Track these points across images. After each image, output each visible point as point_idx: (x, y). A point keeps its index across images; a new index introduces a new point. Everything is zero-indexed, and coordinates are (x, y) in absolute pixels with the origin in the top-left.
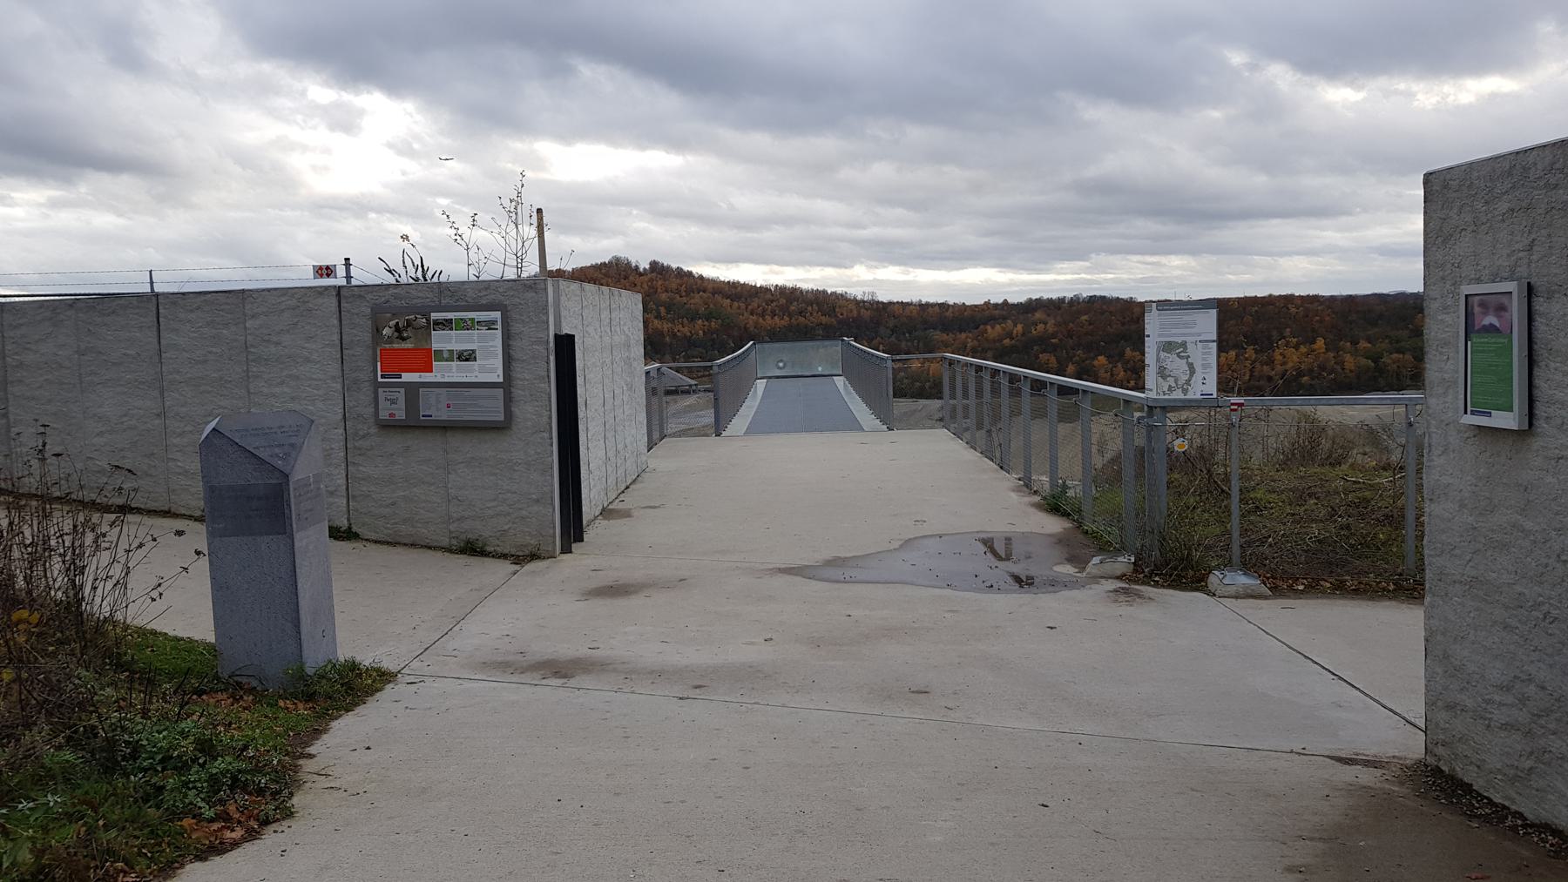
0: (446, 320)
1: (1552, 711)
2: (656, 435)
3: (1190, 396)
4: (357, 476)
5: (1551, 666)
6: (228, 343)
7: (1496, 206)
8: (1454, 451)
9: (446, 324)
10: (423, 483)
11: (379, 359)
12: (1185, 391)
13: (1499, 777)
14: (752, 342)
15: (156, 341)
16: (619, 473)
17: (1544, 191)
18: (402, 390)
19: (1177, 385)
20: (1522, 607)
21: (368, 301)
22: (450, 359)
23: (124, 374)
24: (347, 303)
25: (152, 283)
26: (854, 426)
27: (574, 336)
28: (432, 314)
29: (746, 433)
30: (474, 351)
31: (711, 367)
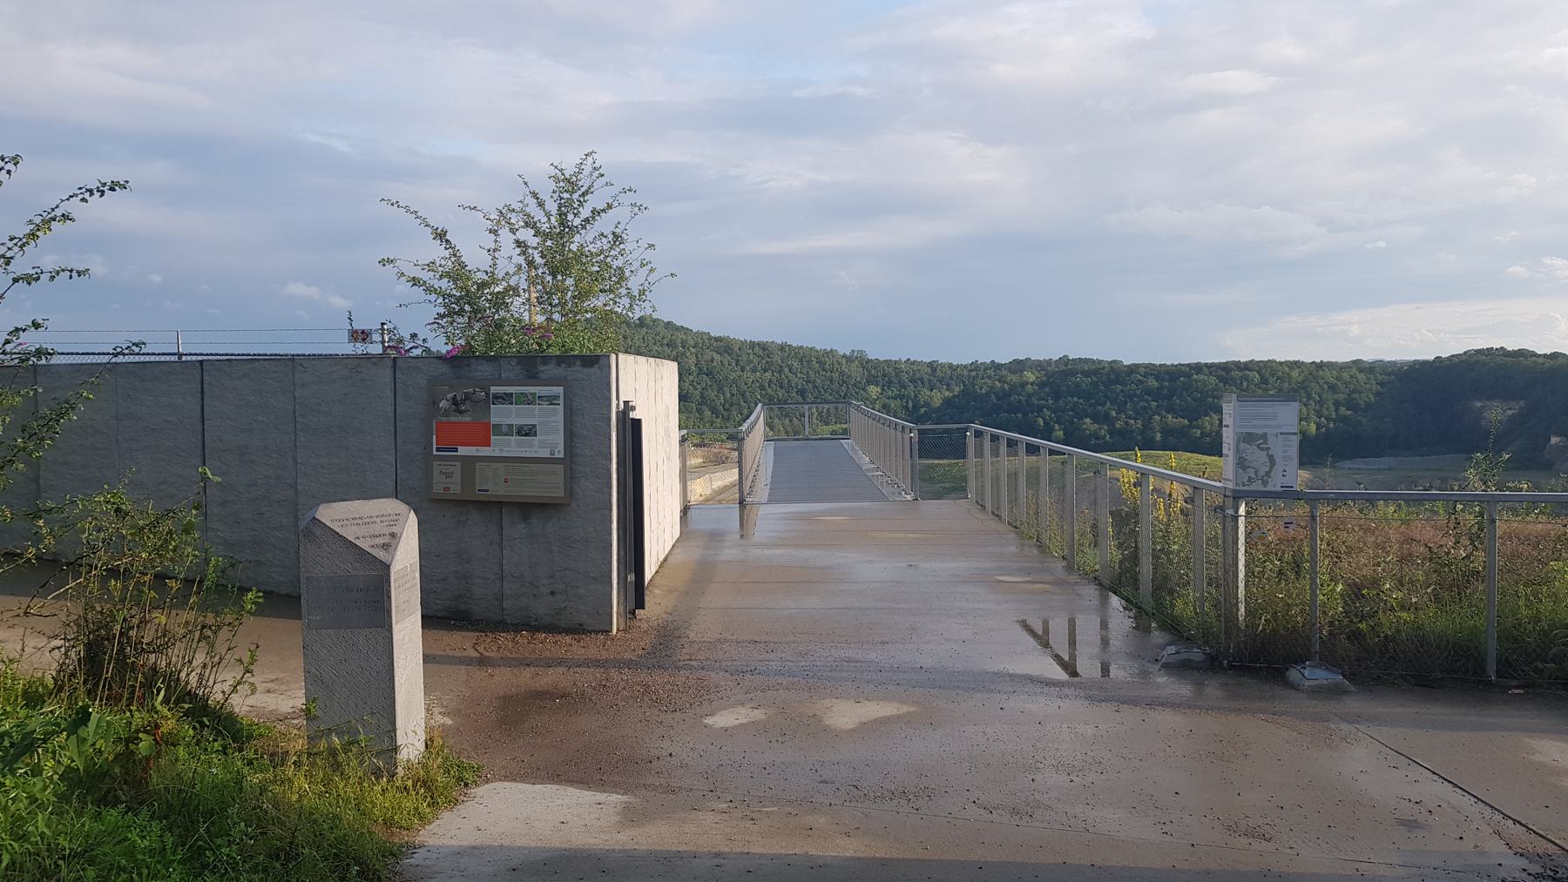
0: (506, 394)
3: (1270, 488)
9: (506, 398)
12: (1265, 483)
28: (492, 388)
30: (534, 426)
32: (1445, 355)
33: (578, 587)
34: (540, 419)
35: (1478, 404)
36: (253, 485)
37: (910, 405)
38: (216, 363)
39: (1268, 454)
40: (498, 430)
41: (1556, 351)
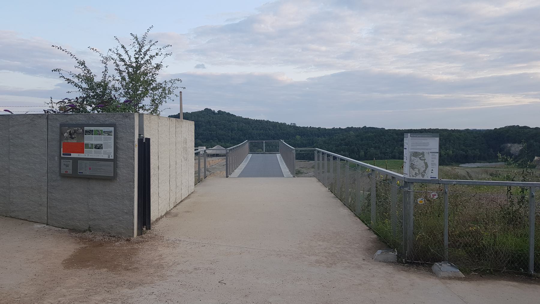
0: (91, 130)
3: (425, 178)
9: (90, 132)
12: (423, 176)
14: (247, 140)
18: (71, 161)
19: (419, 172)
22: (91, 148)
27: (150, 139)
29: (239, 176)
30: (102, 145)
32: (498, 128)
33: (119, 216)
34: (104, 142)
35: (509, 145)
37: (311, 142)
39: (424, 162)
40: (87, 146)
41: (537, 127)
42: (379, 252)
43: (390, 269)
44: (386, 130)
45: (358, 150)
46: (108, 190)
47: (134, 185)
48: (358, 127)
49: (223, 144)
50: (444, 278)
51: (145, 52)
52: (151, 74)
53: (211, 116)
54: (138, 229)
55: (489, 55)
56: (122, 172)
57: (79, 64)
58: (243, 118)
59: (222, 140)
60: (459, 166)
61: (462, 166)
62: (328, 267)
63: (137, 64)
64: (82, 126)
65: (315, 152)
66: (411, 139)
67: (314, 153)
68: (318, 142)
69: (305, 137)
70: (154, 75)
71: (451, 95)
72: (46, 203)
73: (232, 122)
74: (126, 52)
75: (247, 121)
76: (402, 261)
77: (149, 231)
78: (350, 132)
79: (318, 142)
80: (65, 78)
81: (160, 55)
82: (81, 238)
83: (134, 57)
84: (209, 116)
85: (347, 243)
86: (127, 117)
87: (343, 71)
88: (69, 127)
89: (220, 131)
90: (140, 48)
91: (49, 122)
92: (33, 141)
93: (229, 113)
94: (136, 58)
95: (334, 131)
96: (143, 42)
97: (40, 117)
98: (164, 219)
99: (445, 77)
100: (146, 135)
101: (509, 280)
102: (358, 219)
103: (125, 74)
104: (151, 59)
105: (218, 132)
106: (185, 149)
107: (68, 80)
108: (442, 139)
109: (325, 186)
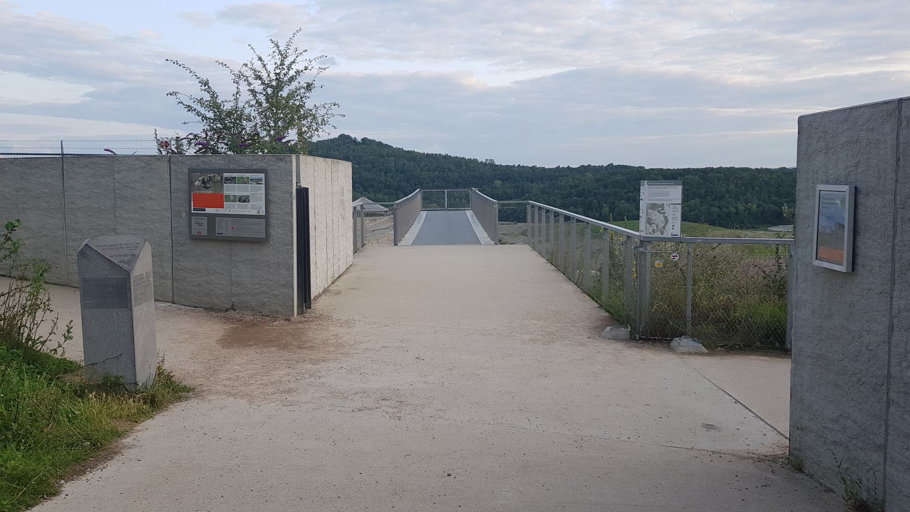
0: (232, 178)
1: (860, 436)
2: (359, 246)
3: (665, 235)
4: (179, 267)
5: (860, 410)
6: (104, 187)
7: (838, 139)
8: (810, 280)
9: (232, 180)
10: (217, 273)
11: (192, 200)
12: (662, 233)
13: (830, 471)
14: (419, 189)
15: (61, 185)
16: (335, 268)
17: (866, 132)
18: (206, 218)
19: (657, 229)
20: (845, 374)
21: (186, 165)
22: (234, 201)
23: (42, 204)
24: (174, 166)
25: (62, 148)
26: (476, 241)
27: (308, 188)
28: (224, 174)
29: (413, 244)
30: (248, 196)
31: (393, 205)
36: (42, 228)
38: (70, 158)
39: (664, 216)
42: (608, 328)
43: (620, 346)
44: (647, 169)
45: (599, 203)
46: (258, 255)
47: (293, 249)
48: (599, 166)
49: (372, 195)
50: (683, 353)
51: (288, 65)
52: (299, 97)
53: (350, 148)
54: (298, 306)
55: (820, 41)
56: (275, 232)
57: (201, 85)
58: (405, 151)
59: (369, 189)
60: (767, 230)
61: (774, 230)
62: (545, 344)
63: (279, 83)
64: (220, 172)
65: (527, 206)
66: (649, 188)
67: (527, 207)
68: (531, 192)
69: (510, 182)
70: (303, 99)
71: (756, 110)
72: (171, 274)
73: (387, 157)
74: (264, 66)
75: (412, 156)
76: (635, 337)
77: (309, 310)
78: (586, 174)
79: (532, 190)
80: (184, 105)
81: (310, 70)
82: (225, 318)
83: (274, 72)
84: (348, 147)
85: (569, 321)
86: (282, 160)
87: (574, 68)
88: (201, 173)
89: (365, 173)
90: (282, 60)
91: (172, 166)
92: (149, 191)
93: (380, 143)
94: (276, 74)
95: (559, 172)
96: (286, 51)
97: (159, 159)
98: (323, 297)
99: (747, 79)
100: (303, 185)
101: (761, 356)
102: (587, 296)
103: (262, 98)
104: (298, 76)
105: (362, 175)
106: (342, 203)
107: (188, 106)
108: (740, 185)
109: (542, 256)
